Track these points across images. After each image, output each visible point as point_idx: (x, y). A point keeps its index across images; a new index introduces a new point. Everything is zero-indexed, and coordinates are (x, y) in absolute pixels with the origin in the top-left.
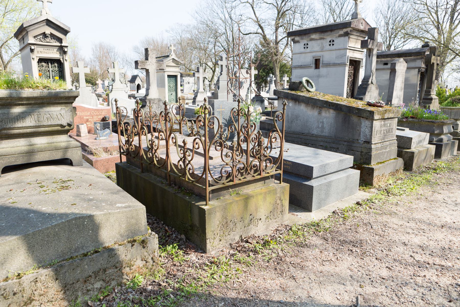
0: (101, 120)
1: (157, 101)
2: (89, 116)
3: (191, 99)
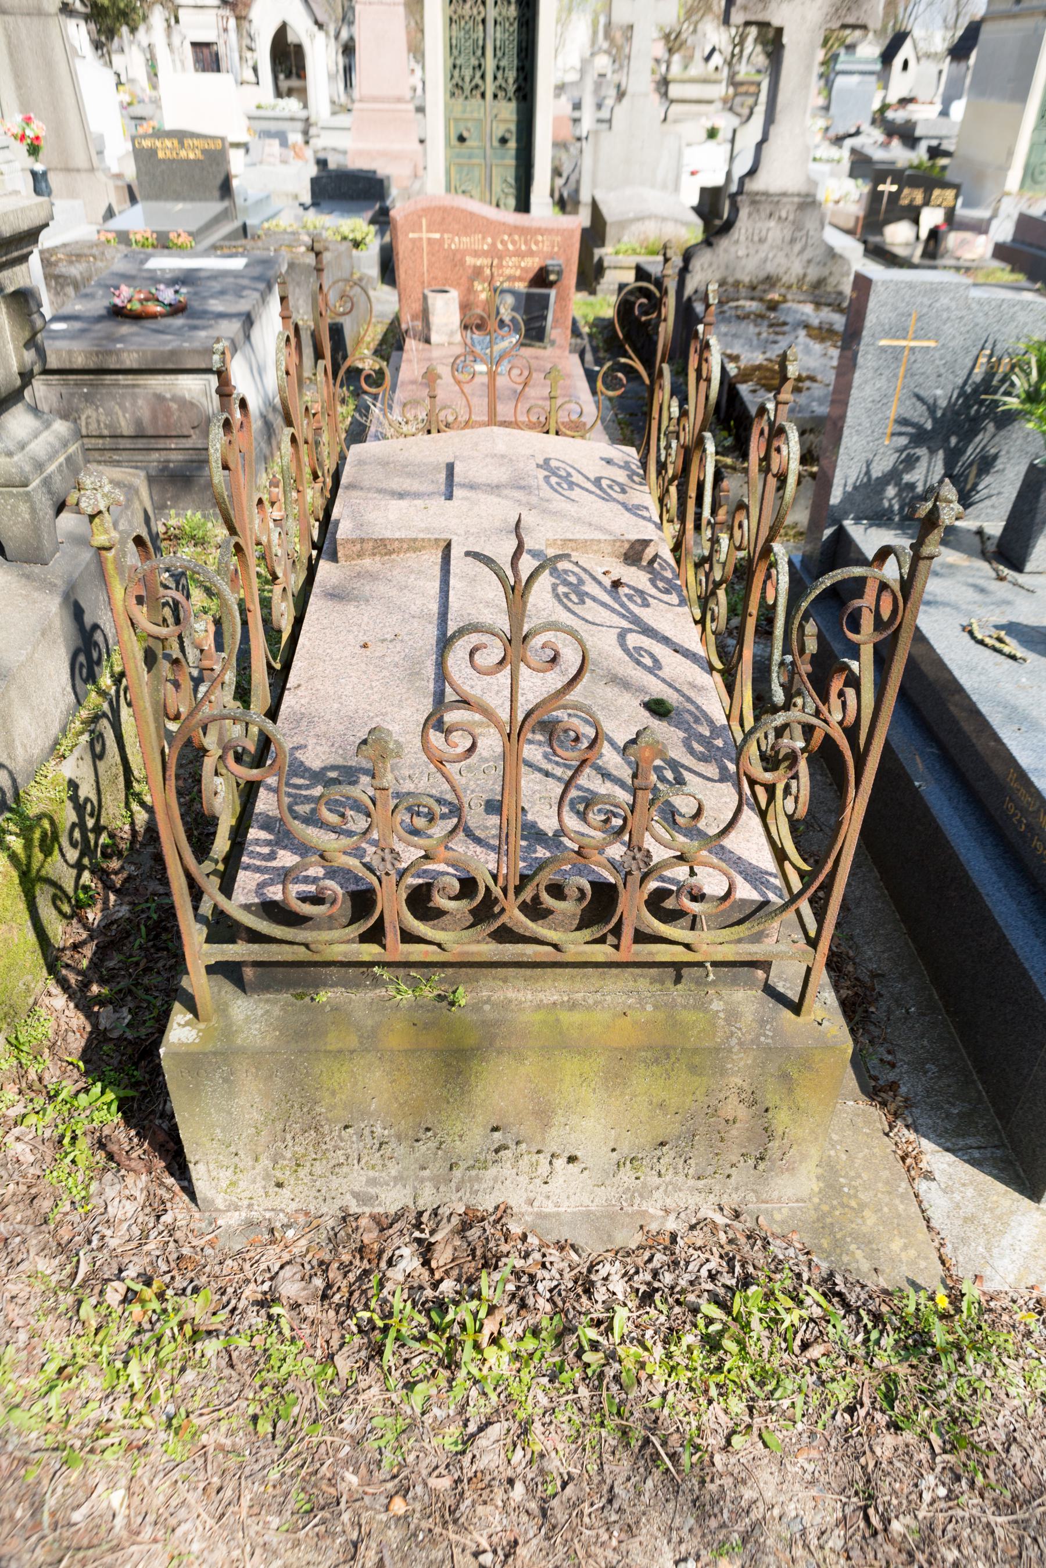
0: (531, 275)
1: (792, 208)
2: (484, 254)
3: (629, 268)
